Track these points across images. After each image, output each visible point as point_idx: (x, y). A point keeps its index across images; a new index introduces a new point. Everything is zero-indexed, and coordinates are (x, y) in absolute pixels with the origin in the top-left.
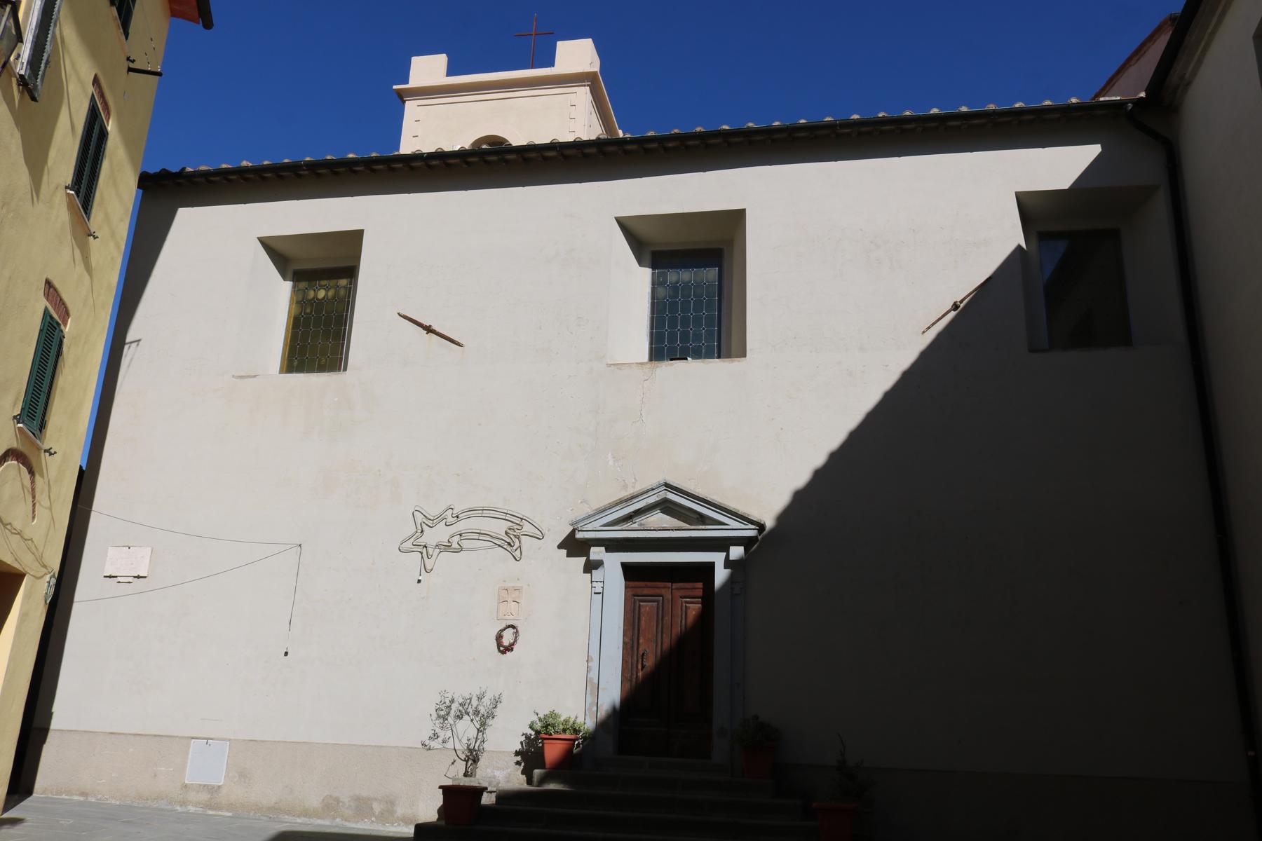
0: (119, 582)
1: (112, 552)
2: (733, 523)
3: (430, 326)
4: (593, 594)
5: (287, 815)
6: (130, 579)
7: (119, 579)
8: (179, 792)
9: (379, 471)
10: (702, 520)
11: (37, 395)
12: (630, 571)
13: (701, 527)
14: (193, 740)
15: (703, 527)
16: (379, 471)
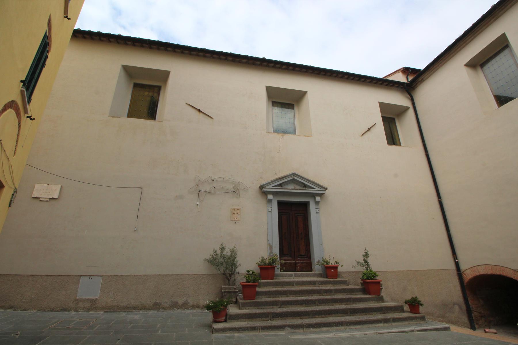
0: (41, 201)
1: (37, 186)
2: (317, 189)
3: (200, 109)
4: (235, 222)
5: (135, 309)
6: (48, 200)
10: (305, 186)
12: (280, 204)
14: (82, 277)
16: (178, 161)
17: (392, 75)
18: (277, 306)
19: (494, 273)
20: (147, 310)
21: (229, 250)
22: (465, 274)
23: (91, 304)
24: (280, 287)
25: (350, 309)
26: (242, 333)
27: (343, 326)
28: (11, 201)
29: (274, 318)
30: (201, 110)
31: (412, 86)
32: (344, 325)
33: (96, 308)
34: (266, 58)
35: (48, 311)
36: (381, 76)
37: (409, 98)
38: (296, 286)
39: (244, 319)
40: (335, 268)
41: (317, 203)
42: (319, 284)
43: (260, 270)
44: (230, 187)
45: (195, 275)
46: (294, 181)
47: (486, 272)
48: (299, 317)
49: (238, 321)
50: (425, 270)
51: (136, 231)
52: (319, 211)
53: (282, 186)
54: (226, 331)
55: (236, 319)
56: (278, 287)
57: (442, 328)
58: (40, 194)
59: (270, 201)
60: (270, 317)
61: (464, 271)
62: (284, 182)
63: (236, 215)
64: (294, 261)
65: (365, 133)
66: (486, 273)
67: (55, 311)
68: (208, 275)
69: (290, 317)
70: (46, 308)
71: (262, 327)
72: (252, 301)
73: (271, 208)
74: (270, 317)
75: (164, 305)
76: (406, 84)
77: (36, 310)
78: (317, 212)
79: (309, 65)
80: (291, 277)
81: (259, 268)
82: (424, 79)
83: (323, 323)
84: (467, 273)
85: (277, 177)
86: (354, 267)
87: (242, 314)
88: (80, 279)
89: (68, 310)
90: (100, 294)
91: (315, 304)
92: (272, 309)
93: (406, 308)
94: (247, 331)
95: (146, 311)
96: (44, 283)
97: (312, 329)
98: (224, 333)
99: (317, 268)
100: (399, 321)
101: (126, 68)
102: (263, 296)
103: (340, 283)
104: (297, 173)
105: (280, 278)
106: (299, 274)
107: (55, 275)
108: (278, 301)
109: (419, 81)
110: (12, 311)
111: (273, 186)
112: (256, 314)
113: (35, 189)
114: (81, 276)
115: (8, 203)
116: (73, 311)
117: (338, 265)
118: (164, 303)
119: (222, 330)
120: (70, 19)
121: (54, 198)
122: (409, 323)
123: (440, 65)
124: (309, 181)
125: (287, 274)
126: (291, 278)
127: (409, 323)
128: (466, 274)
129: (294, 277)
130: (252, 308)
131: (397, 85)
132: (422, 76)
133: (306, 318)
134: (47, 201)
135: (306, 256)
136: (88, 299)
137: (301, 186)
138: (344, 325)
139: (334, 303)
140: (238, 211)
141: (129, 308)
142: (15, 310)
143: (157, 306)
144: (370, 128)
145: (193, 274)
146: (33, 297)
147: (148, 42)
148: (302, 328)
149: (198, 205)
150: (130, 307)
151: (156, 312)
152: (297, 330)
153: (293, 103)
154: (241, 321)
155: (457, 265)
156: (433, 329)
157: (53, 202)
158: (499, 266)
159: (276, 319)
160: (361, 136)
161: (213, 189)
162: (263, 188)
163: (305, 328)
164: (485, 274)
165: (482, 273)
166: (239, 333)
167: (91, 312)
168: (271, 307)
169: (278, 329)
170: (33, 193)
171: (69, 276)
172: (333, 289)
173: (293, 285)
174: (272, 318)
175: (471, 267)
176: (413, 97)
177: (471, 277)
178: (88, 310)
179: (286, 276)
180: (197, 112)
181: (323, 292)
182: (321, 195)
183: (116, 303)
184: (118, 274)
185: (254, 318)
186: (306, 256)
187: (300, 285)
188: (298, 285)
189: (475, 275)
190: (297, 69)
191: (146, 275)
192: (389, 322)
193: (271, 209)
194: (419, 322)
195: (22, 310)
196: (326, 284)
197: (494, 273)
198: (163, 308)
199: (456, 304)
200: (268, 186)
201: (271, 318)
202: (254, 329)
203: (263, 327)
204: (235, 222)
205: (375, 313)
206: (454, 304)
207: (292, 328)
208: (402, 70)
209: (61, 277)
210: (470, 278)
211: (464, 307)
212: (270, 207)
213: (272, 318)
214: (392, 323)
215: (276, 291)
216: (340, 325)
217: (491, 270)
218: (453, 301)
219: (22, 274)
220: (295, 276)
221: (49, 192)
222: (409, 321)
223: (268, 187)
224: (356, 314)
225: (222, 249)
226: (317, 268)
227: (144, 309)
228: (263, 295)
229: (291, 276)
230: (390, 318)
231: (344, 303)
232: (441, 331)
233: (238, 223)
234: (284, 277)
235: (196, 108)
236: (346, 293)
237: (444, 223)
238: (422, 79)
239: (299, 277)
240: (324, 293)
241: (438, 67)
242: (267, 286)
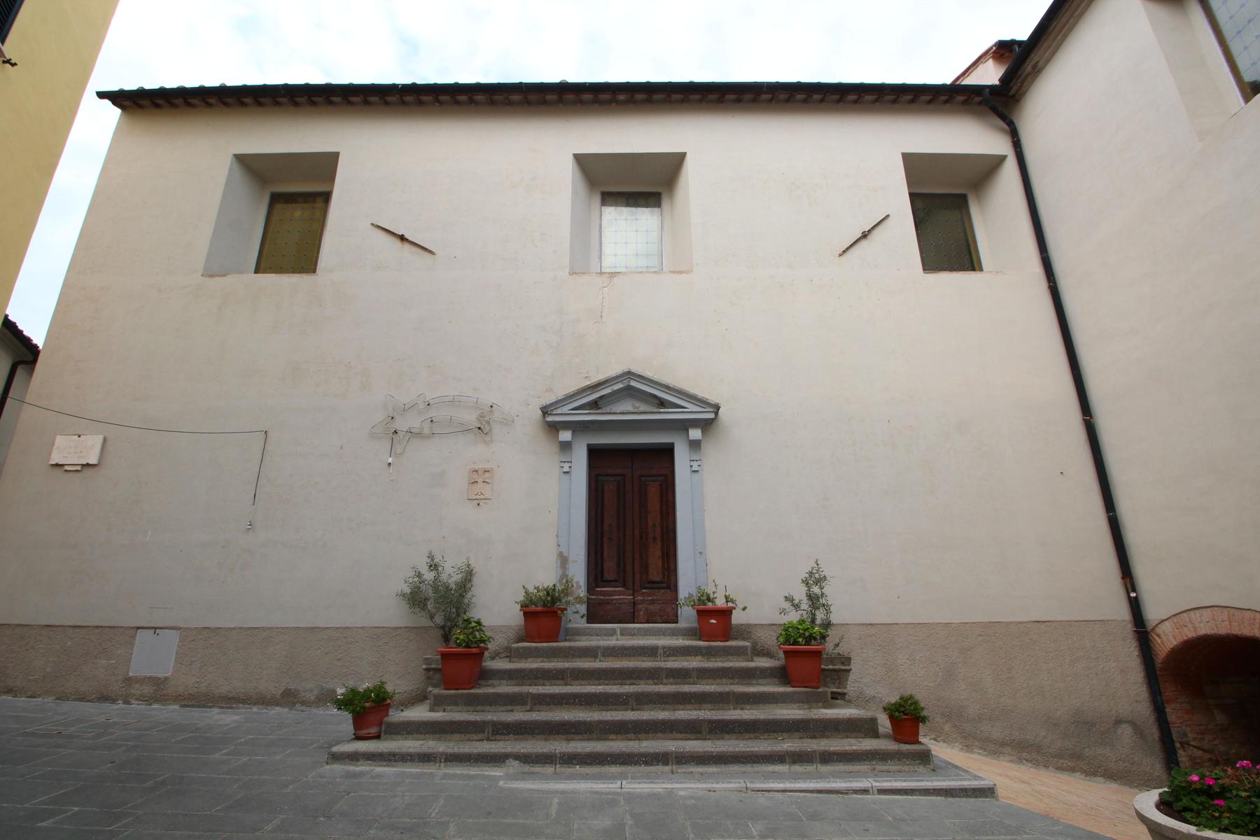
0: (66, 471)
1: (60, 440)
2: (692, 408)
4: (478, 502)
5: (242, 703)
6: (79, 468)
7: (67, 468)
8: (121, 685)
9: (350, 363)
10: (662, 403)
11: (6, 12)
12: (595, 454)
13: (662, 410)
14: (139, 631)
15: (666, 410)
17: (970, 71)
18: (523, 707)
19: (1236, 630)
20: (267, 705)
21: (454, 570)
22: (1159, 636)
23: (155, 688)
24: (560, 659)
25: (710, 722)
26: (396, 766)
27: (668, 765)
29: (496, 735)
30: (407, 236)
31: (1011, 94)
32: (670, 762)
33: (166, 698)
34: (569, 81)
35: (76, 700)
36: (946, 78)
37: (1003, 130)
39: (423, 735)
40: (725, 614)
41: (695, 445)
42: (668, 656)
44: (470, 418)
45: (377, 629)
46: (630, 392)
47: (1213, 629)
48: (563, 736)
49: (406, 739)
50: (1021, 623)
51: (250, 529)
52: (699, 466)
53: (600, 408)
54: (358, 760)
55: (403, 734)
56: (556, 660)
57: (966, 789)
58: (64, 457)
59: (566, 447)
60: (487, 731)
61: (1157, 625)
62: (604, 395)
63: (480, 485)
64: (632, 597)
65: (852, 245)
66: (1213, 632)
67: (88, 701)
68: (407, 630)
69: (539, 734)
70: (70, 693)
71: (446, 754)
72: (461, 691)
73: (570, 464)
74: (488, 732)
75: (304, 697)
76: (987, 90)
77: (54, 698)
79: (941, 83)
80: (612, 635)
81: (522, 613)
82: (1040, 64)
83: (610, 755)
84: (1164, 633)
85: (588, 383)
86: (783, 612)
87: (418, 722)
88: (136, 632)
89: (112, 700)
90: (174, 667)
91: (627, 704)
92: (508, 714)
93: (884, 723)
94: (409, 764)
95: (267, 709)
96: (69, 643)
97: (578, 767)
98: (353, 765)
99: (687, 615)
100: (840, 761)
101: (243, 161)
102: (505, 681)
103: (739, 652)
104: (637, 369)
105: (584, 638)
107: (88, 627)
108: (528, 694)
109: (1025, 73)
110: (11, 698)
112: (452, 723)
113: (55, 447)
114: (138, 628)
116: (120, 702)
117: (733, 605)
118: (304, 692)
119: (348, 757)
120: (15, 64)
121: (90, 463)
122: (874, 769)
123: (1076, 15)
124: (668, 388)
125: (600, 629)
126: (611, 638)
127: (874, 769)
128: (1162, 635)
129: (615, 636)
130: (459, 708)
131: (946, 98)
132: (1033, 55)
133: (583, 740)
134: (77, 471)
135: (664, 585)
136: (150, 678)
137: (646, 402)
138: (670, 764)
139: (681, 704)
140: (487, 475)
141: (229, 699)
142: (16, 696)
143: (289, 698)
144: (869, 231)
145: (372, 628)
146: (48, 670)
147: (283, 92)
148: (551, 763)
149: (390, 464)
150: (233, 698)
151: (286, 710)
152: (538, 769)
153: (660, 191)
154: (413, 739)
155: (1135, 606)
156: (934, 790)
157: (88, 472)
158: (1249, 610)
159: (503, 737)
160: (840, 255)
161: (427, 425)
162: (546, 415)
163: (560, 763)
164: (1212, 635)
165: (1205, 633)
166: (388, 766)
167: (155, 706)
168: (509, 708)
169: (488, 762)
170: (52, 455)
171: (114, 627)
172: (693, 668)
173: (595, 656)
174: (493, 734)
175: (1173, 614)
176: (1017, 125)
177: (1175, 643)
178: (149, 700)
179: (598, 633)
180: (398, 243)
181: (664, 676)
183: (205, 688)
184: (320, 626)
185: (446, 733)
186: (664, 585)
187: (613, 656)
188: (608, 656)
189: (1185, 638)
190: (656, 97)
191: (268, 628)
192: (808, 762)
193: (570, 467)
194: (907, 768)
195: (28, 697)
196: (685, 656)
197: (1235, 633)
198: (303, 703)
199: (1125, 722)
200: (559, 409)
201: (490, 736)
202: (426, 758)
203: (450, 755)
204: (478, 502)
205: (785, 735)
206: (1118, 722)
207: (524, 763)
208: (994, 52)
209: (100, 630)
210: (1171, 647)
211: (1154, 732)
213: (493, 734)
214: (819, 765)
215: (537, 668)
216: (659, 762)
217: (1227, 623)
218: (1113, 712)
219: (29, 623)
220: (622, 634)
222: (874, 763)
223: (559, 411)
224: (727, 736)
225: (434, 567)
226: (687, 615)
227: (262, 704)
228: (504, 679)
229: (612, 633)
230: (814, 751)
231: (709, 706)
232: (960, 797)
233: (485, 503)
234: (593, 637)
235: (395, 232)
236: (730, 678)
238: (1035, 66)
239: (633, 635)
240: (667, 678)
241: (1072, 21)
242: (526, 658)
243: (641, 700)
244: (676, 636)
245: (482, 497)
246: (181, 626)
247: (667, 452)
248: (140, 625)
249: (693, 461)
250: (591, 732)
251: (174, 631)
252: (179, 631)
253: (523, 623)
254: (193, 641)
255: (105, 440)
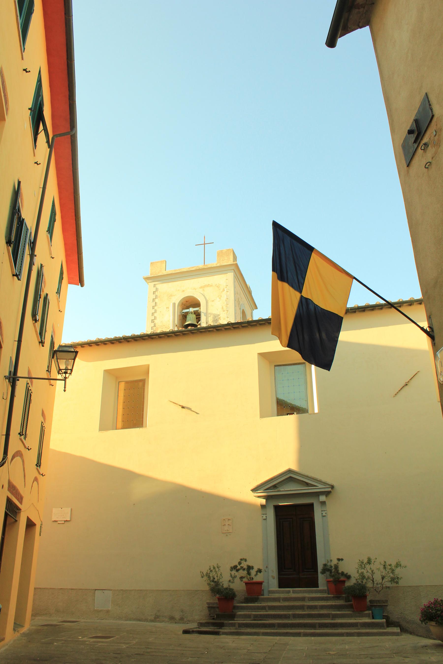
0: (59, 523)
1: (54, 510)
2: (320, 486)
6: (63, 522)
7: (59, 522)
10: (307, 484)
14: (96, 591)
28: (40, 531)
38: (282, 602)
43: (245, 586)
73: (266, 515)
78: (324, 514)
106: (298, 590)
111: (264, 489)
113: (53, 513)
114: (96, 590)
115: (39, 535)
121: (68, 520)
124: (307, 477)
140: (230, 522)
157: (66, 523)
160: (394, 397)
182: (327, 494)
191: (145, 590)
212: (265, 514)
221: (63, 515)
229: (289, 592)
233: (230, 535)
237: (277, 559)
243: (295, 616)
244: (317, 593)
245: (228, 532)
246: (112, 589)
247: (311, 506)
248: (96, 588)
249: (323, 511)
250: (275, 627)
251: (109, 591)
252: (111, 591)
253: (245, 589)
254: (117, 595)
255: (71, 510)
